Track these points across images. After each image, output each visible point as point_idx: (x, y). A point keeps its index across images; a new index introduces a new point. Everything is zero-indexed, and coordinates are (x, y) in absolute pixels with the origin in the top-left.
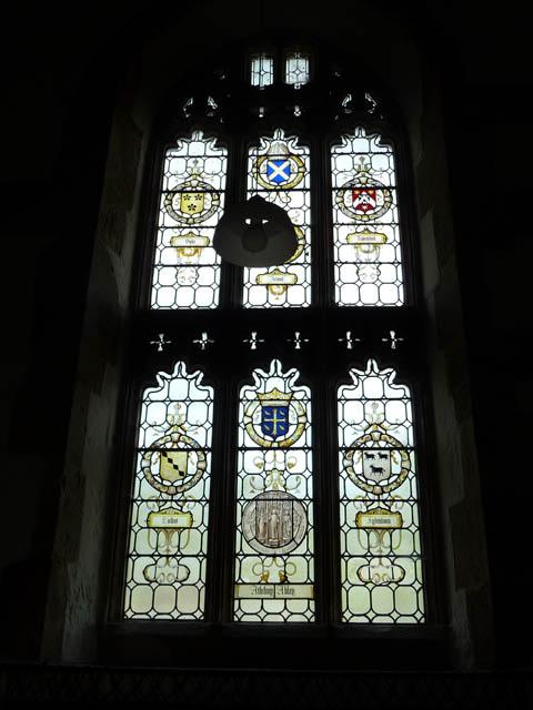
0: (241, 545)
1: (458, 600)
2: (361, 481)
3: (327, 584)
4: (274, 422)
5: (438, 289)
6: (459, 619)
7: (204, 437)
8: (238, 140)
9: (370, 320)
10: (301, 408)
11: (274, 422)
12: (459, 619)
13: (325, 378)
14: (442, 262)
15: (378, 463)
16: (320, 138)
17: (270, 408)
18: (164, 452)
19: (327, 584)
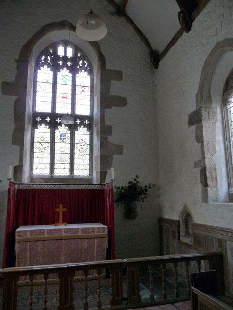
0: (56, 161)
1: (94, 172)
2: (79, 150)
3: (54, 106)
4: (63, 137)
5: (96, 114)
6: (94, 176)
7: (88, 142)
8: (55, 68)
9: (83, 118)
10: (68, 135)
11: (63, 137)
12: (94, 176)
13: (73, 128)
14: (98, 109)
15: (82, 147)
16: (74, 70)
17: (62, 135)
18: (40, 143)
19: (54, 106)
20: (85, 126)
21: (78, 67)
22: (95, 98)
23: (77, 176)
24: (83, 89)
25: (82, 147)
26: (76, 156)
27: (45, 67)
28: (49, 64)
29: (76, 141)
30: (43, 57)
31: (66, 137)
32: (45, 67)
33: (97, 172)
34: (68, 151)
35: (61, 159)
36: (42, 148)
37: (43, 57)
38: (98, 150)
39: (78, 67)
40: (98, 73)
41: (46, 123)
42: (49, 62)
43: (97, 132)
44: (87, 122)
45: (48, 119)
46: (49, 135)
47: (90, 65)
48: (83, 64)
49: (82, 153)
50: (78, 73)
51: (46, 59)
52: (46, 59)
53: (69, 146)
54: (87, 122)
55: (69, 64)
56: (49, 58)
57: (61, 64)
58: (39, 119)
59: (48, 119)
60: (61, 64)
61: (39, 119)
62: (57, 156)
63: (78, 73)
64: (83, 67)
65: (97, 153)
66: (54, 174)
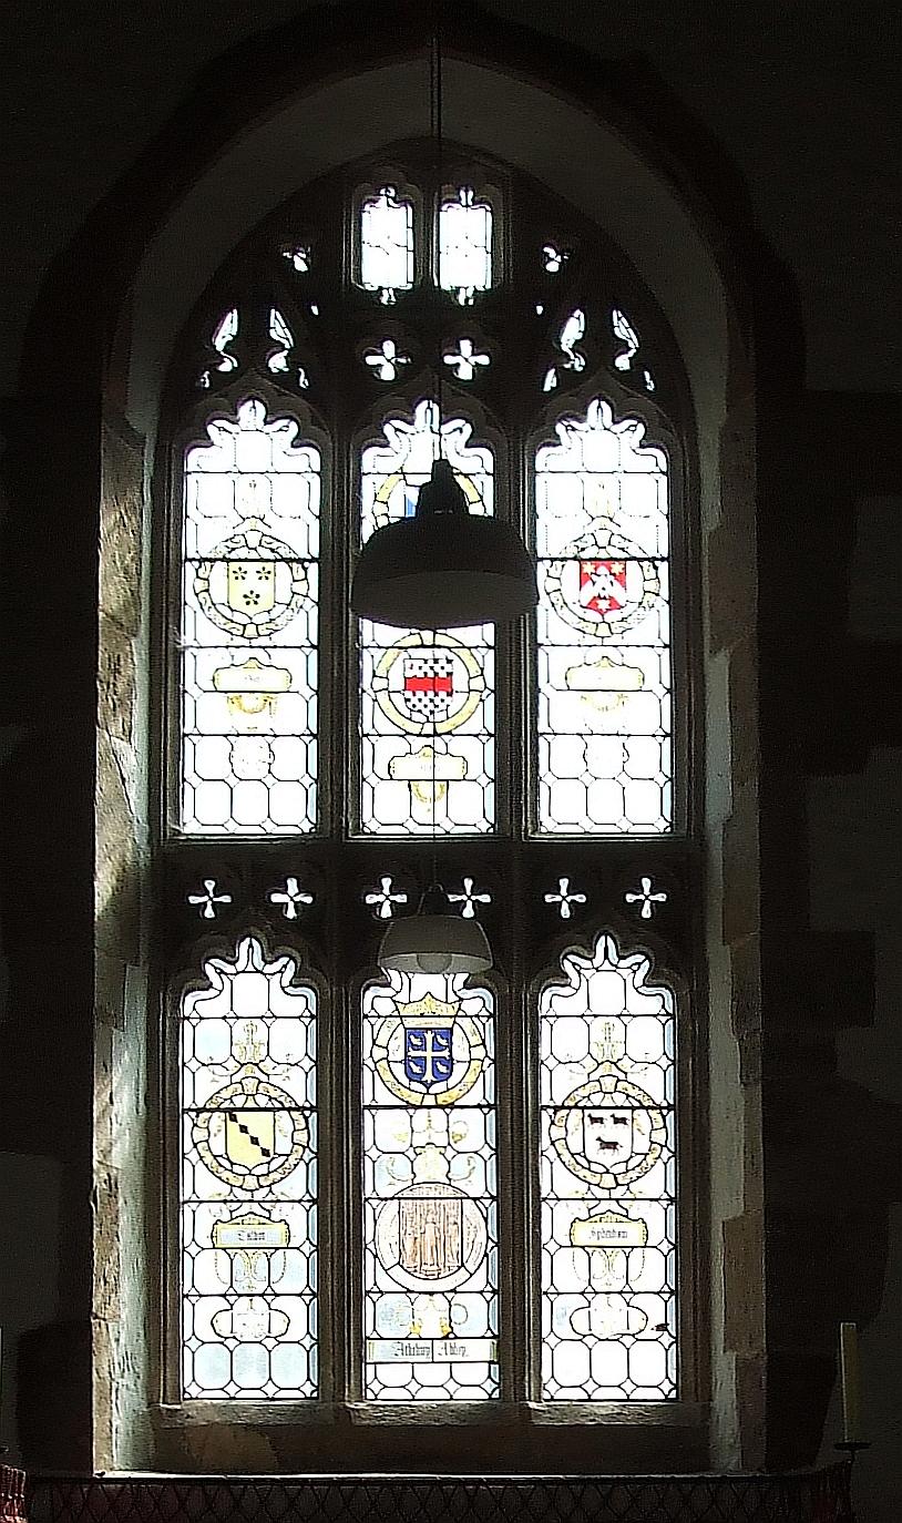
1: (724, 1367)
10: (473, 1046)
14: (738, 779)
15: (610, 1131)
17: (419, 1032)
20: (631, 936)
21: (550, 381)
22: (718, 670)
23: (398, 1409)
24: (603, 583)
25: (610, 1131)
26: (556, 1222)
27: (599, 414)
28: (286, 380)
29: (557, 1084)
30: (229, 327)
31: (460, 1051)
32: (599, 414)
33: (743, 1368)
34: (479, 1178)
35: (419, 1252)
36: (248, 1155)
37: (229, 327)
38: (750, 1164)
39: (550, 381)
40: (729, 436)
41: (279, 937)
42: (278, 362)
43: (739, 995)
44: (647, 898)
45: (290, 897)
46: (293, 1041)
47: (658, 349)
48: (599, 342)
49: (610, 1195)
50: (555, 441)
51: (253, 343)
52: (253, 343)
53: (475, 1129)
54: (647, 898)
55: (466, 361)
56: (278, 330)
57: (388, 374)
58: (208, 901)
59: (290, 897)
60: (388, 374)
61: (564, 898)
62: (382, 1230)
63: (555, 441)
64: (249, 381)
65: (731, 1197)
66: (361, 1388)
